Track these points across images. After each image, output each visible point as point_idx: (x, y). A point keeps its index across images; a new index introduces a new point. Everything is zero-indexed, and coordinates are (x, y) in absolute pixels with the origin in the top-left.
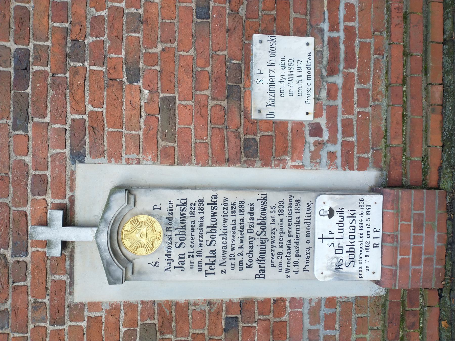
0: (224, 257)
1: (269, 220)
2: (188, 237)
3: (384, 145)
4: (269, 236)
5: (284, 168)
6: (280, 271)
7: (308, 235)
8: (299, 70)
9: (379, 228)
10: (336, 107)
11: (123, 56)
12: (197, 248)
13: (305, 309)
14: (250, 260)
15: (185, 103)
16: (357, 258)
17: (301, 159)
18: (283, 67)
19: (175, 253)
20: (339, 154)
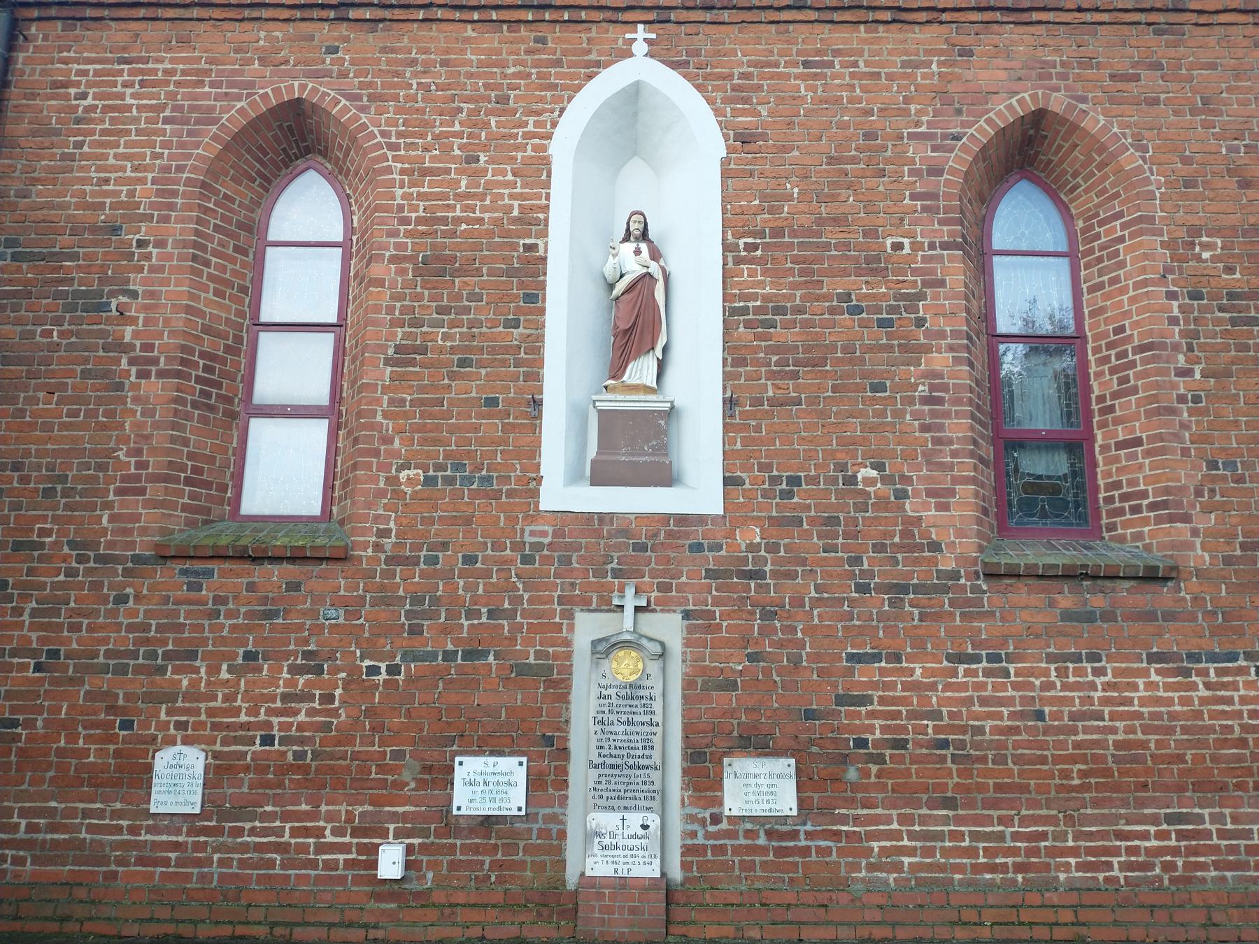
0: (607, 732)
1: (638, 772)
2: (625, 702)
3: (705, 887)
4: (625, 772)
5: (682, 788)
6: (595, 783)
7: (625, 808)
8: (768, 801)
9: (632, 874)
10: (737, 838)
11: (768, 649)
12: (615, 710)
13: (557, 810)
14: (604, 756)
15: (734, 698)
16: (606, 853)
17: (690, 804)
18: (769, 786)
19: (612, 692)
20: (695, 842)
